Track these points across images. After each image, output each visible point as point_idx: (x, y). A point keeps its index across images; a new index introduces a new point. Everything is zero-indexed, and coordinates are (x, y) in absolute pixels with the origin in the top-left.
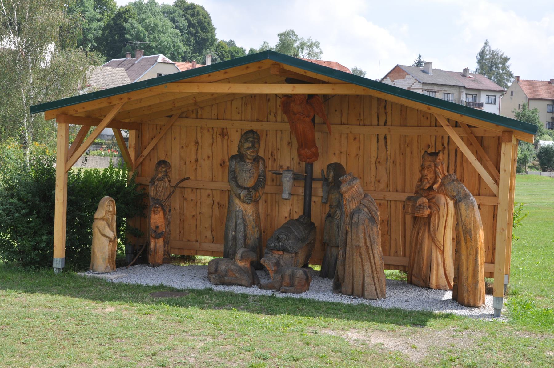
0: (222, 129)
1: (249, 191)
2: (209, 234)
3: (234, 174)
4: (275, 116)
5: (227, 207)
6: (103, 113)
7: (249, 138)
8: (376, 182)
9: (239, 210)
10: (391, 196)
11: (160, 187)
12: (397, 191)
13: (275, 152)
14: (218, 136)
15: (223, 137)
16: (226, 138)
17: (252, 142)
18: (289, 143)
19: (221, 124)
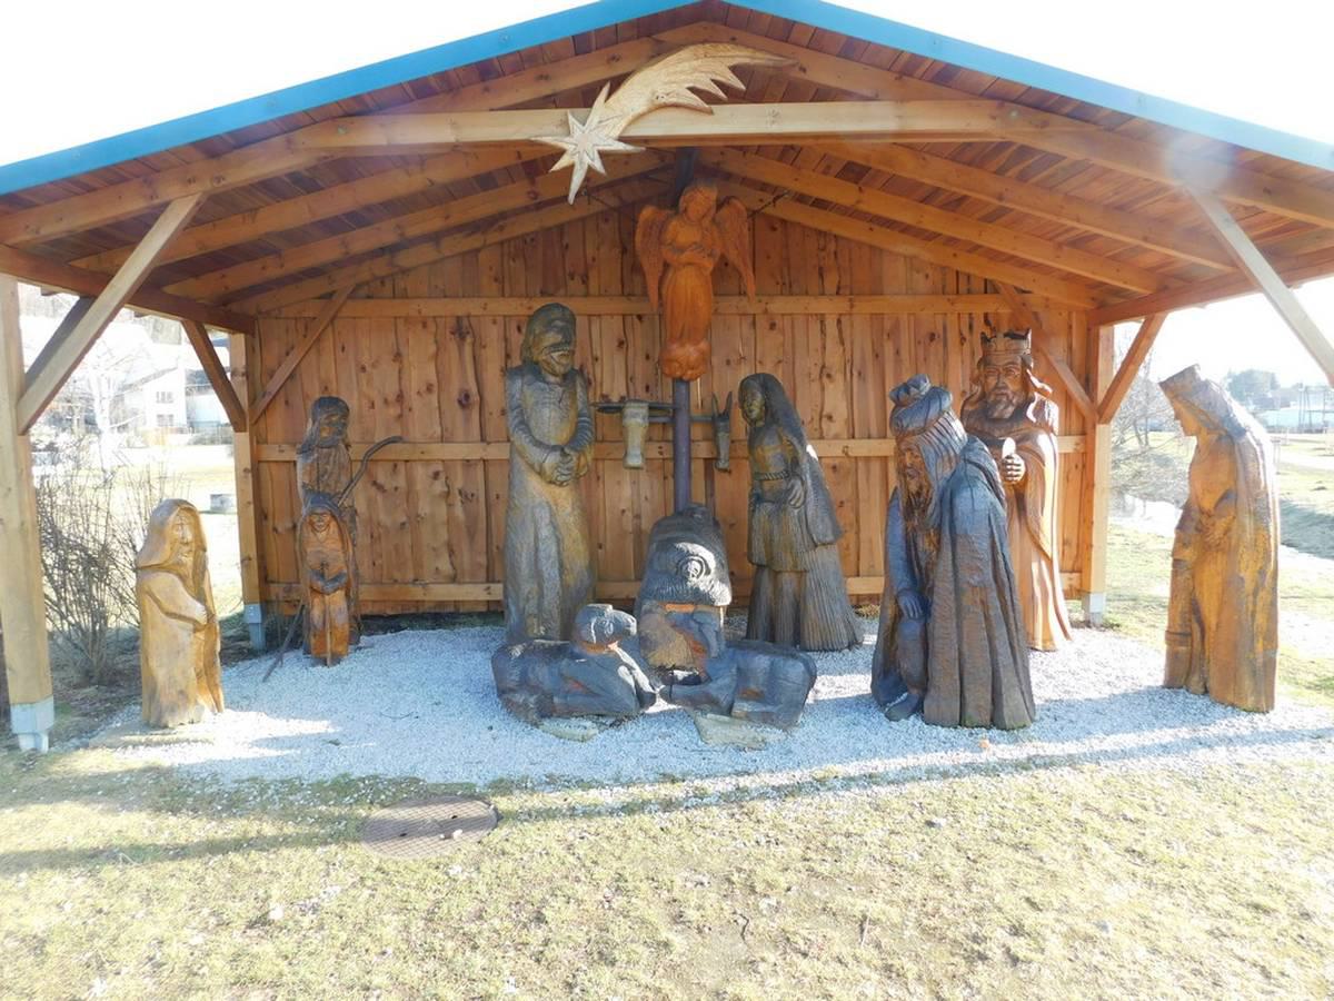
0: (459, 319)
1: (564, 454)
2: (445, 565)
3: (521, 413)
4: (584, 282)
5: (482, 499)
6: (123, 236)
7: (553, 320)
8: (824, 419)
9: (540, 504)
10: (860, 448)
11: (328, 463)
12: (869, 437)
13: (590, 365)
14: (448, 335)
15: (463, 338)
16: (469, 339)
17: (561, 330)
18: (621, 343)
19: (460, 307)
